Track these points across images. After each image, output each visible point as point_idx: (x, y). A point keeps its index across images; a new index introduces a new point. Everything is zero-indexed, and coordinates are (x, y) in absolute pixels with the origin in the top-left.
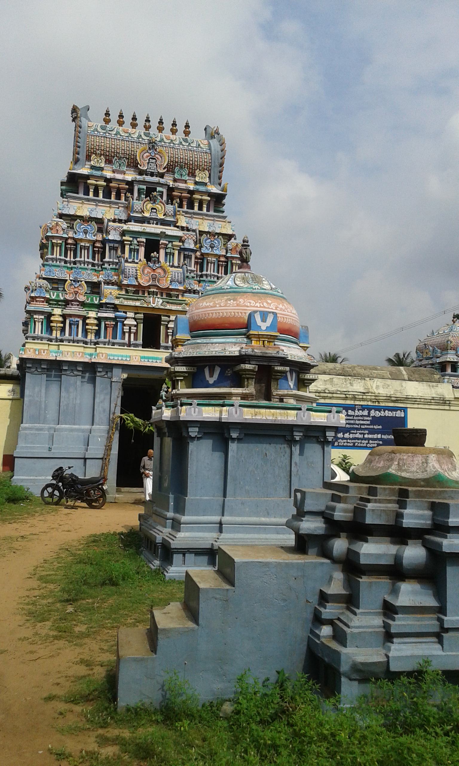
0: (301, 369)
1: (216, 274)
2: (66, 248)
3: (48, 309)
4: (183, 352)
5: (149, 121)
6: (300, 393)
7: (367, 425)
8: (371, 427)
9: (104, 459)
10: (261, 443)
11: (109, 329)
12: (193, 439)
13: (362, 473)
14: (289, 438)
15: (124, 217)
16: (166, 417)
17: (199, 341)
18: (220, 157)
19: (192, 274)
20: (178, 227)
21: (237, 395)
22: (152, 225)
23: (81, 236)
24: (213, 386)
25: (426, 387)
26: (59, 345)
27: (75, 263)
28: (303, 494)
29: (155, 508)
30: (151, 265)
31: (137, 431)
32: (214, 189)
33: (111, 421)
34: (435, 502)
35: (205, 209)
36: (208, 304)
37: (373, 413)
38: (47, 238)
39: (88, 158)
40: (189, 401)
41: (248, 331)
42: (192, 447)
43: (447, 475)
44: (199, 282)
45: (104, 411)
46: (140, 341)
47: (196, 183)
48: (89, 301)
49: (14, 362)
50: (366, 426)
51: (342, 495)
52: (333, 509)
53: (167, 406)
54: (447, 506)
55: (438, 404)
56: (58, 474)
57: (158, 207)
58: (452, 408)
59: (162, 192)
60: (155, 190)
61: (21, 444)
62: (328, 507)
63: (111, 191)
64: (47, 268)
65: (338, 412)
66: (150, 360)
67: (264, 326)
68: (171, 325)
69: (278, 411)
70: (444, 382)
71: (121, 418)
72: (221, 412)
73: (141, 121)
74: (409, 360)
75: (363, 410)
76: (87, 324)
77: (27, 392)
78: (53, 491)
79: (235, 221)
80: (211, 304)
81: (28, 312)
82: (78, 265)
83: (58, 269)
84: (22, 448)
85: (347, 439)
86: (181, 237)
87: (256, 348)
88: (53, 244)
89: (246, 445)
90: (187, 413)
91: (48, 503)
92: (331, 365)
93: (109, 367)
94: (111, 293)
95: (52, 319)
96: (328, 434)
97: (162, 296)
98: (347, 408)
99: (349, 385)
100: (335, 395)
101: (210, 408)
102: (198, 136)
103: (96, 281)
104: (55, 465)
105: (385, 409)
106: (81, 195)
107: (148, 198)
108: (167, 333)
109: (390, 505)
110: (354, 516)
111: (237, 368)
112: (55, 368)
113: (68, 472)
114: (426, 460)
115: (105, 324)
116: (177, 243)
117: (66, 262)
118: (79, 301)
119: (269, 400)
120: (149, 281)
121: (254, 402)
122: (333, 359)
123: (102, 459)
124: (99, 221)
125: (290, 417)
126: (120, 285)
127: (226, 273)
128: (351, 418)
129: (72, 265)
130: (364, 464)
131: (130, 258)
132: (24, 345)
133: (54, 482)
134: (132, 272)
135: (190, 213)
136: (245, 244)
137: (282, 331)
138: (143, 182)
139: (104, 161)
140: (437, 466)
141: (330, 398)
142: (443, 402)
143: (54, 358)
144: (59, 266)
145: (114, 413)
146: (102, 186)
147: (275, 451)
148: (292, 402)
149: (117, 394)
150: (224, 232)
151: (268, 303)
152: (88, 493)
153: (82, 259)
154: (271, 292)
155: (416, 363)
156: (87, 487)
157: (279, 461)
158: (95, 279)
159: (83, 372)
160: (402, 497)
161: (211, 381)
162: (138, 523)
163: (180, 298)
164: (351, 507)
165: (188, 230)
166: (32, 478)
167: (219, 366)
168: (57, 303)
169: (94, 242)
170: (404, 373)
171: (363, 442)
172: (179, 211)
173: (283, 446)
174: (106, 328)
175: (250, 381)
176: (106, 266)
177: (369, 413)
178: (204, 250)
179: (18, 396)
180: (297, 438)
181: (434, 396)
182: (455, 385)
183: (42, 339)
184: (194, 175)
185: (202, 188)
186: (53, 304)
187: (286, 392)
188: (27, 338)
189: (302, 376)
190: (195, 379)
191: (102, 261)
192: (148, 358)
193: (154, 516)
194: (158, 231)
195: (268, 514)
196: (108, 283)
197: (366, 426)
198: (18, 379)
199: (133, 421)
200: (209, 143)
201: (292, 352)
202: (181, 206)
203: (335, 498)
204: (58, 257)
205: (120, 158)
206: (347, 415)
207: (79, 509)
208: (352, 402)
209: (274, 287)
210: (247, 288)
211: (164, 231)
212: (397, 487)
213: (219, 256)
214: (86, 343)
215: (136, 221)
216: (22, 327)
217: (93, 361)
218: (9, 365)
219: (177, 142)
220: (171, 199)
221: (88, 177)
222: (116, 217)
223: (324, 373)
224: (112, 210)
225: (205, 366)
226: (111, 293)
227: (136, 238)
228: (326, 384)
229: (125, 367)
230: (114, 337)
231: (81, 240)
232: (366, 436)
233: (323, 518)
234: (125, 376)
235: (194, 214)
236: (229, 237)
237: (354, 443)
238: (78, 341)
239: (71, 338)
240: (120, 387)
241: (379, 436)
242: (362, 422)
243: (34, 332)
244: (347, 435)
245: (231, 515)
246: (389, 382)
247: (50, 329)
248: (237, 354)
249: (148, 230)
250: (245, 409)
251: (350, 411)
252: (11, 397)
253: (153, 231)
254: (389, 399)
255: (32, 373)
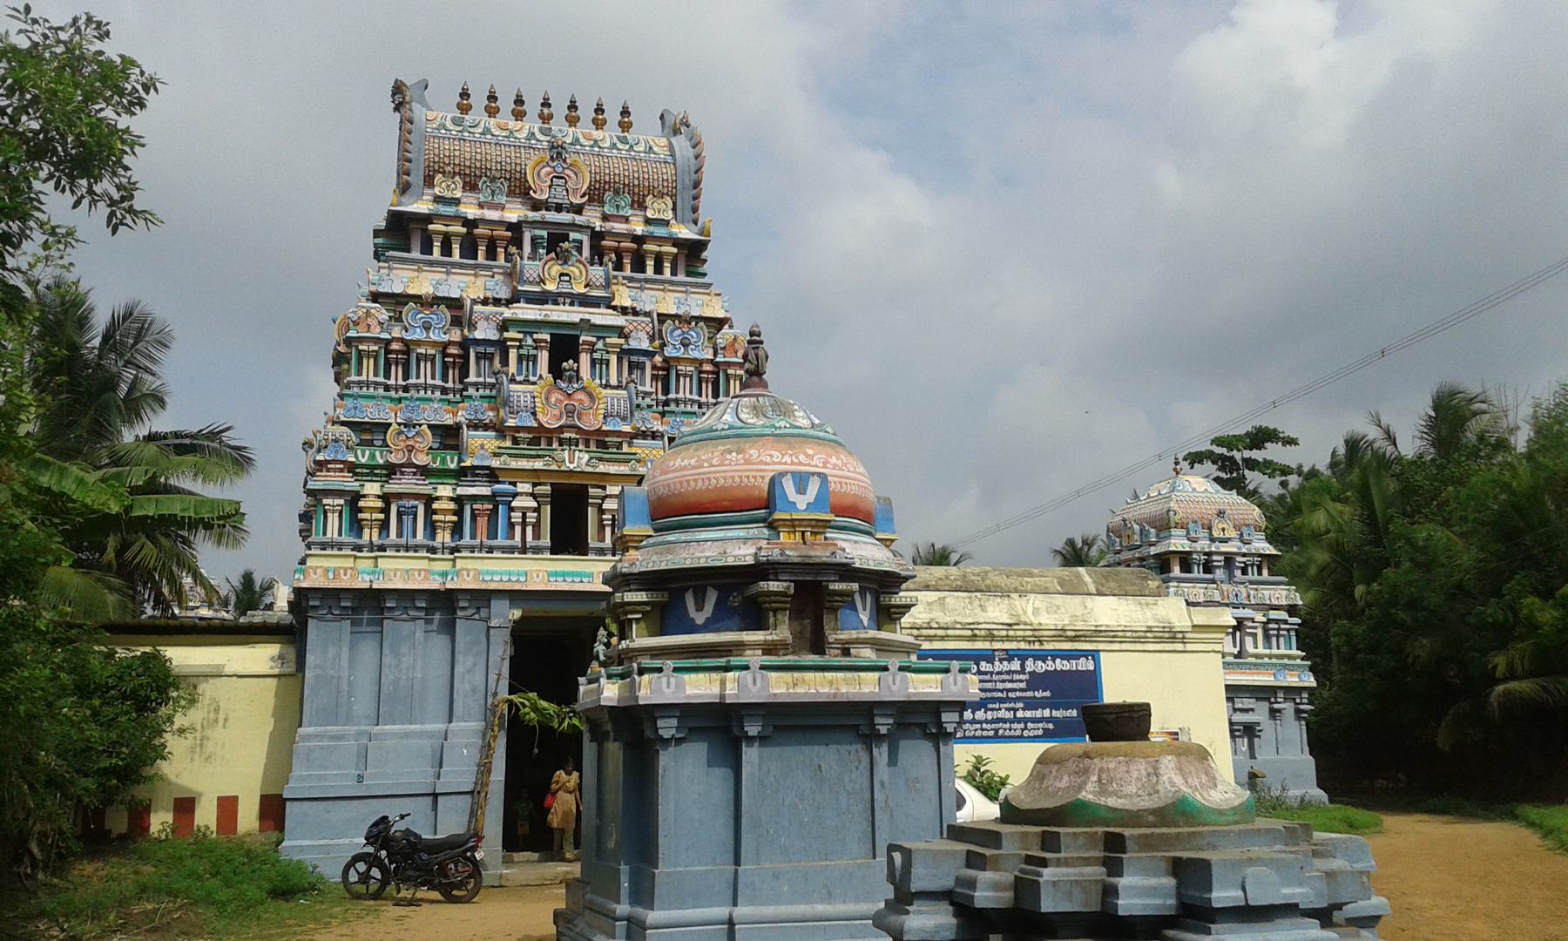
0: (883, 587)
1: (696, 397)
2: (387, 360)
3: (351, 484)
4: (639, 561)
5: (549, 105)
6: (883, 635)
7: (1022, 690)
8: (1030, 694)
9: (477, 794)
10: (808, 743)
11: (481, 518)
12: (666, 742)
13: (1025, 802)
14: (865, 730)
15: (504, 293)
16: (610, 699)
17: (671, 538)
18: (693, 169)
19: (648, 401)
20: (614, 308)
21: (754, 645)
22: (561, 307)
23: (418, 334)
24: (705, 628)
25: (1132, 607)
26: (376, 558)
27: (406, 389)
28: (907, 854)
29: (588, 896)
30: (563, 385)
31: (546, 729)
32: (685, 232)
33: (489, 711)
34: (1180, 859)
35: (667, 271)
36: (686, 462)
37: (1030, 665)
38: (349, 342)
39: (429, 181)
40: (657, 663)
41: (771, 514)
42: (666, 760)
43: (1199, 797)
44: (663, 414)
45: (474, 691)
46: (546, 541)
47: (648, 221)
48: (437, 465)
49: (282, 597)
50: (1018, 694)
51: (988, 852)
52: (972, 884)
53: (609, 677)
54: (1205, 865)
55: (1160, 640)
56: (379, 833)
57: (574, 270)
58: (1189, 647)
59: (581, 242)
60: (565, 238)
61: (298, 770)
62: (959, 881)
63: (475, 243)
64: (349, 402)
65: (963, 671)
66: (569, 579)
67: (802, 502)
68: (610, 505)
69: (840, 675)
70: (1167, 595)
71: (511, 704)
72: (723, 683)
73: (532, 106)
74: (1094, 552)
75: (1010, 659)
76: (435, 512)
77: (311, 659)
78: (369, 870)
79: (728, 294)
80: (693, 462)
81: (310, 493)
82: (413, 392)
83: (371, 403)
84: (302, 778)
85: (980, 722)
86: (622, 328)
87: (788, 547)
88: (360, 354)
89: (777, 749)
90: (651, 690)
91: (358, 897)
92: (938, 571)
93: (482, 598)
94: (482, 446)
95: (361, 504)
96: (945, 717)
97: (587, 446)
98: (978, 657)
99: (978, 610)
100: (950, 632)
101: (701, 675)
102: (648, 137)
103: (450, 422)
104: (370, 812)
105: (1055, 654)
106: (416, 254)
107: (553, 255)
108: (601, 521)
109: (1088, 870)
110: (1016, 898)
111: (753, 590)
112: (369, 606)
113: (400, 826)
114: (1156, 769)
115: (473, 510)
116: (615, 340)
117: (387, 388)
118: (416, 466)
119: (822, 653)
120: (560, 418)
121: (791, 659)
122: (940, 558)
123: (471, 793)
124: (454, 304)
125: (865, 686)
126: (500, 430)
127: (716, 395)
128: (988, 677)
129: (401, 394)
130: (1028, 782)
131: (520, 373)
132: (303, 562)
133: (370, 849)
134: (525, 400)
135: (639, 281)
136: (755, 340)
137: (839, 511)
138: (543, 224)
139: (460, 186)
140: (1178, 780)
141: (942, 638)
142: (1171, 635)
143: (367, 586)
144: (373, 397)
145: (495, 694)
146: (457, 234)
147: (836, 760)
148: (867, 654)
149: (500, 652)
150: (708, 313)
151: (807, 455)
152: (443, 871)
153: (422, 380)
154: (812, 432)
155: (1110, 558)
156: (441, 857)
157: (846, 778)
158: (449, 420)
159: (429, 610)
160: (1113, 850)
161: (700, 619)
162: (553, 930)
163: (625, 449)
164: (1007, 877)
165: (635, 313)
166: (322, 842)
167: (715, 587)
168: (371, 471)
169: (445, 345)
170: (1087, 579)
171: (1014, 726)
172: (615, 277)
173: (853, 748)
174: (474, 517)
175: (779, 616)
176: (471, 391)
177: (1023, 666)
178: (669, 352)
179: (291, 668)
180: (883, 730)
181: (1151, 623)
182: (1191, 599)
183: (340, 546)
184: (642, 206)
185: (659, 231)
186: (362, 475)
187: (854, 634)
188: (309, 547)
189: (884, 600)
190: (666, 617)
191: (461, 382)
192: (564, 574)
193: (587, 912)
194: (576, 318)
195: (829, 897)
196: (475, 426)
197: (1018, 694)
198: (291, 633)
199: (535, 709)
200: (671, 144)
201: (863, 552)
202: (619, 266)
203: (974, 861)
204: (372, 378)
205: (493, 179)
206: (979, 672)
207: (425, 906)
208: (987, 645)
209: (817, 421)
210: (763, 426)
211: (587, 317)
212: (1100, 830)
213: (701, 362)
214: (433, 550)
215: (529, 301)
216: (298, 525)
217: (449, 586)
218: (268, 600)
219: (607, 144)
220: (598, 254)
221: (428, 218)
222: (489, 294)
223: (927, 588)
224: (480, 281)
225: (686, 590)
226: (482, 446)
227: (531, 334)
228: (931, 611)
229: (515, 596)
230: (493, 534)
231: (419, 343)
232: (1020, 714)
233: (952, 904)
234: (517, 614)
235: (647, 281)
236: (718, 324)
237: (997, 731)
238: (416, 548)
239: (403, 541)
240: (508, 638)
241: (1047, 713)
242: (1009, 686)
243: (325, 534)
244: (980, 715)
245: (752, 903)
246: (1059, 599)
247: (357, 526)
248: (750, 561)
249: (554, 317)
250: (773, 675)
251: (983, 664)
252: (276, 671)
253: (564, 318)
254: (1061, 634)
255: (320, 619)
